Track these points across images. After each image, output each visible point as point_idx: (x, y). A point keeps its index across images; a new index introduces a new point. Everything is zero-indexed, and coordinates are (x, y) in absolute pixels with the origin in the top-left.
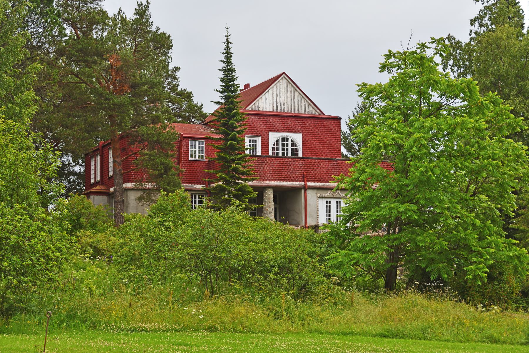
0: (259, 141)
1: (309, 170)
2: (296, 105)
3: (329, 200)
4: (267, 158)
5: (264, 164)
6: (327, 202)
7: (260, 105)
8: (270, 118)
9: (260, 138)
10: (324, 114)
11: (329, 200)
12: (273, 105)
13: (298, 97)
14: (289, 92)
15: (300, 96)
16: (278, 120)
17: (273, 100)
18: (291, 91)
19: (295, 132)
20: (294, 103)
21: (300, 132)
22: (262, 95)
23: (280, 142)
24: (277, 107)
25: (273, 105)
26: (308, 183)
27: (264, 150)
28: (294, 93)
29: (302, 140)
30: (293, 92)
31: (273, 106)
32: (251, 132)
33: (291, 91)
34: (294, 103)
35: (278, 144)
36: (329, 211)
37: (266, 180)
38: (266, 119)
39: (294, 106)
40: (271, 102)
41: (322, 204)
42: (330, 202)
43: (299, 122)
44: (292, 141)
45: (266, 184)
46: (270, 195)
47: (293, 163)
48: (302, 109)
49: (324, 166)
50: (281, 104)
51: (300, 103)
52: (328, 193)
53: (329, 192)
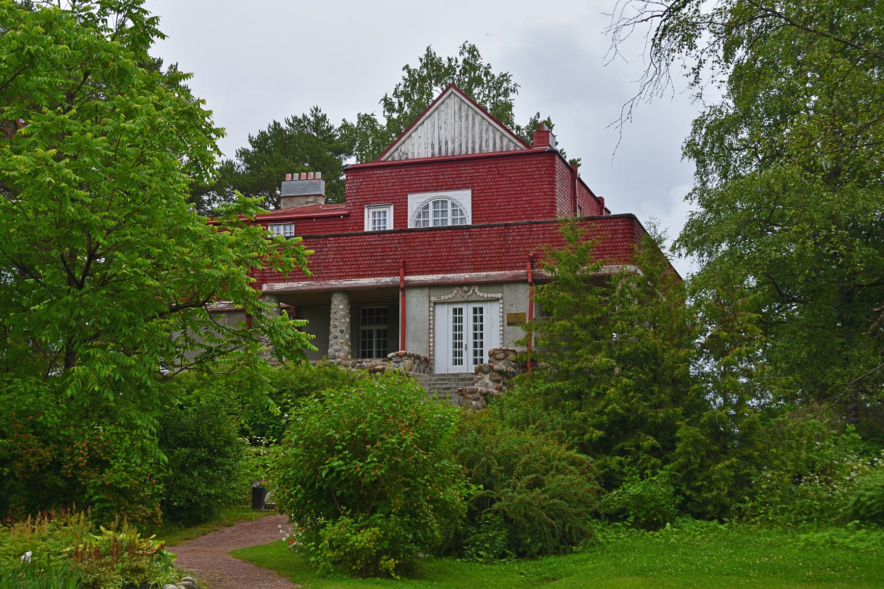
0: (390, 211)
1: (413, 252)
2: (477, 140)
3: (458, 306)
4: (332, 239)
5: (326, 249)
6: (455, 311)
8: (410, 169)
9: (392, 207)
11: (458, 306)
12: (432, 145)
13: (481, 124)
14: (463, 119)
15: (485, 122)
16: (425, 170)
18: (467, 116)
19: (458, 189)
20: (473, 136)
21: (468, 188)
22: (411, 131)
23: (431, 209)
24: (440, 149)
25: (432, 145)
26: (407, 278)
27: (403, 224)
28: (473, 118)
29: (472, 201)
30: (470, 118)
31: (433, 148)
32: (376, 199)
33: (467, 116)
34: (473, 136)
36: (458, 328)
37: (330, 278)
39: (474, 143)
40: (430, 141)
41: (444, 316)
42: (461, 310)
43: (466, 171)
44: (453, 205)
45: (330, 286)
46: (339, 309)
47: (381, 243)
48: (487, 146)
49: (442, 242)
50: (446, 143)
51: (484, 134)
53: (455, 292)
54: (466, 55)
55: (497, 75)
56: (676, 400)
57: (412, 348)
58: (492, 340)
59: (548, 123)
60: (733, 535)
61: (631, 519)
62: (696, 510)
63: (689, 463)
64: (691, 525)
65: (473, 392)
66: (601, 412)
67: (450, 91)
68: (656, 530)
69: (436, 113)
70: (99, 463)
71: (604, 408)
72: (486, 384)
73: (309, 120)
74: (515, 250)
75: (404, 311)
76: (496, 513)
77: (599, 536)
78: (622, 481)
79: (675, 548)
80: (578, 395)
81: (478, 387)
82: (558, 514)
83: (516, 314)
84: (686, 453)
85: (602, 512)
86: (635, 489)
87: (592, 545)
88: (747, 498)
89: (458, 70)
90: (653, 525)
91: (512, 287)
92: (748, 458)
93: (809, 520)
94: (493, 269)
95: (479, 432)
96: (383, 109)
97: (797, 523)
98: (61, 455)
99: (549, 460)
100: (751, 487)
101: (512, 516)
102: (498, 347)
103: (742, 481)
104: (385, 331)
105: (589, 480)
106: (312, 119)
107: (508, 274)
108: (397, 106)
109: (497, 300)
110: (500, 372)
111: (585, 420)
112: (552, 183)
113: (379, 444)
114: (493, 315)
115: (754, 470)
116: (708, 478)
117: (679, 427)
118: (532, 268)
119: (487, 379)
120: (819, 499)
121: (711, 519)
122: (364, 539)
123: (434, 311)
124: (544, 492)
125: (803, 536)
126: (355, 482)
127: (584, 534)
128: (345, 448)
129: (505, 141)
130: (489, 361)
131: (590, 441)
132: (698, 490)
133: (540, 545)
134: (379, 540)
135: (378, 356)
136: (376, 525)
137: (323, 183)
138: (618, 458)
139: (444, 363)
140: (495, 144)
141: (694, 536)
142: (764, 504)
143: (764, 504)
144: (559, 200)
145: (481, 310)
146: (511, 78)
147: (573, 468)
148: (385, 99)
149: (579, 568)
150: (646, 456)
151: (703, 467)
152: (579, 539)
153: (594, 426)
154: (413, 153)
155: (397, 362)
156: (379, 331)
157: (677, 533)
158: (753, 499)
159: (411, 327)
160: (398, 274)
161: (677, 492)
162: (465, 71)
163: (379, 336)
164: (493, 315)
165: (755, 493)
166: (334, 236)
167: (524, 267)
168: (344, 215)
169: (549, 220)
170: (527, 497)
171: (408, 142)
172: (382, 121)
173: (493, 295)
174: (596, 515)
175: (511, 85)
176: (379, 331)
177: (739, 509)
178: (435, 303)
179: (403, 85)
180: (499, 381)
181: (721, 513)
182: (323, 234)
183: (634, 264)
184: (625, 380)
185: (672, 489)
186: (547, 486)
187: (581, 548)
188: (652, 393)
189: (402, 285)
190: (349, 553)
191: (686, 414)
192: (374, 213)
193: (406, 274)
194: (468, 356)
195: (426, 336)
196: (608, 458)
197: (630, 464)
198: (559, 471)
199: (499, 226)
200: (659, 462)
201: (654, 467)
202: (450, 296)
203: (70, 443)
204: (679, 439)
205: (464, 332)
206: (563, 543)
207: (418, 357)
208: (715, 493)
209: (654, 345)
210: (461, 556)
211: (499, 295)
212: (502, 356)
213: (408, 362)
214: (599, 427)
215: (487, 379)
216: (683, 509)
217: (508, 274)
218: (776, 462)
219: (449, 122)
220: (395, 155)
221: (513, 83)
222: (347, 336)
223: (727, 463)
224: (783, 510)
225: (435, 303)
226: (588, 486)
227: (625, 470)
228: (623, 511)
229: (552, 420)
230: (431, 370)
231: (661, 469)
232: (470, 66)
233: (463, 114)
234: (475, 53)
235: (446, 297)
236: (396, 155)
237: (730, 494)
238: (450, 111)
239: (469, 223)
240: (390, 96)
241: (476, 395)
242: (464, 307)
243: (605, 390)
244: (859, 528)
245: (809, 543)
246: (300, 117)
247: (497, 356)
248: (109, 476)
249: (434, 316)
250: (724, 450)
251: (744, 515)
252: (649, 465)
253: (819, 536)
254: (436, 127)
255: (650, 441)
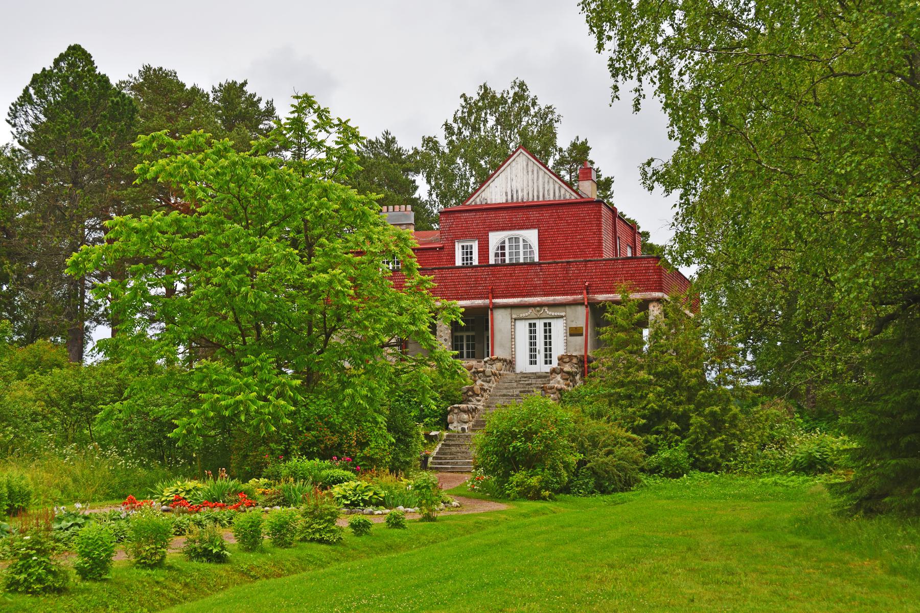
0: (475, 245)
6: (530, 325)
7: (489, 195)
9: (477, 242)
10: (582, 197)
11: (532, 321)
12: (506, 193)
13: (543, 178)
14: (530, 173)
15: (546, 176)
16: (503, 214)
17: (507, 187)
18: (533, 171)
19: (527, 229)
20: (538, 187)
21: (535, 228)
24: (512, 196)
25: (506, 193)
28: (538, 173)
31: (507, 195)
33: (533, 171)
34: (538, 187)
35: (503, 248)
36: (532, 337)
38: (485, 215)
39: (538, 192)
40: (504, 190)
41: (522, 328)
42: (535, 324)
43: (534, 215)
48: (549, 195)
50: (517, 191)
51: (546, 185)
52: (530, 312)
53: (530, 311)
54: (517, 89)
55: (543, 107)
56: (690, 400)
57: (499, 353)
58: (558, 349)
59: (584, 143)
60: (722, 480)
61: (663, 472)
62: (701, 466)
63: (697, 438)
64: (697, 474)
65: (552, 388)
66: (644, 408)
67: (519, 152)
68: (678, 478)
69: (509, 167)
70: (362, 445)
71: (646, 405)
72: (558, 382)
73: (382, 143)
74: (575, 280)
75: (492, 325)
76: (588, 469)
77: (645, 481)
78: (657, 450)
79: (688, 488)
80: (629, 397)
81: (552, 383)
82: (622, 469)
83: (576, 328)
84: (695, 432)
85: (646, 468)
86: (665, 455)
87: (642, 486)
88: (732, 459)
89: (510, 101)
90: (676, 475)
91: (573, 307)
92: (734, 436)
93: (767, 471)
94: (558, 294)
95: (575, 423)
96: (444, 133)
97: (760, 473)
98: (341, 440)
99: (616, 438)
100: (734, 452)
101: (597, 470)
102: (563, 353)
103: (729, 449)
104: (473, 337)
105: (639, 450)
106: (384, 141)
107: (570, 298)
108: (456, 130)
109: (562, 317)
110: (568, 373)
111: (634, 413)
112: (599, 225)
113: (539, 434)
114: (559, 328)
115: (736, 442)
116: (708, 447)
117: (691, 417)
118: (588, 293)
119: (559, 377)
120: (774, 459)
121: (711, 472)
122: (534, 481)
123: (514, 325)
124: (615, 457)
125: (761, 480)
126: (526, 452)
127: (638, 481)
128: (522, 437)
129: (563, 191)
130: (559, 364)
131: (638, 425)
132: (703, 454)
133: (613, 486)
134: (541, 482)
135: (468, 357)
136: (538, 475)
137: (413, 214)
138: (655, 436)
139: (522, 364)
140: (554, 193)
141: (700, 481)
142: (741, 462)
143: (741, 462)
144: (604, 237)
145: (550, 324)
146: (555, 110)
147: (629, 443)
148: (446, 124)
149: (636, 498)
150: (671, 434)
151: (706, 441)
152: (634, 483)
153: (640, 416)
154: (492, 200)
155: (491, 365)
156: (468, 337)
157: (690, 480)
158: (735, 459)
159: (498, 337)
160: (487, 298)
161: (691, 456)
162: (515, 101)
163: (468, 340)
164: (559, 328)
165: (737, 456)
166: (438, 269)
167: (581, 293)
168: (440, 248)
169: (599, 259)
170: (606, 460)
171: (488, 190)
172: (443, 143)
173: (559, 314)
174: (642, 470)
175: (555, 117)
176: (468, 337)
177: (727, 465)
178: (515, 319)
179: (460, 111)
180: (567, 379)
181: (717, 468)
182: (430, 267)
183: (662, 292)
184: (659, 388)
185: (687, 454)
186: (616, 453)
187: (635, 488)
188: (675, 395)
189: (491, 306)
190: (526, 489)
191: (696, 409)
192: (463, 247)
193: (494, 298)
194: (541, 358)
195: (510, 343)
196: (649, 436)
197: (662, 439)
198: (622, 445)
199: (562, 262)
200: (679, 438)
201: (676, 441)
202: (527, 314)
203: (345, 432)
204: (692, 424)
205: (537, 341)
206: (625, 486)
207: (505, 360)
208: (713, 456)
209: (676, 366)
210: (569, 493)
211: (563, 314)
212: (567, 360)
213: (499, 365)
214: (643, 417)
215: (559, 377)
216: (694, 466)
217: (570, 298)
218: (750, 437)
219: (519, 175)
220: (477, 200)
221: (556, 114)
222: (450, 344)
223: (720, 438)
224: (753, 466)
225: (515, 319)
226: (639, 453)
227: (659, 443)
228: (658, 467)
229: (614, 413)
230: (514, 368)
231: (681, 442)
232: (519, 97)
233: (530, 169)
234: (524, 87)
235: (524, 315)
236: (478, 200)
237: (722, 456)
238: (520, 167)
239: (537, 259)
240: (450, 121)
241: (554, 390)
242: (537, 322)
243: (647, 394)
244: (793, 474)
245: (763, 483)
246: (374, 140)
247: (565, 360)
248: (366, 451)
249: (515, 329)
250: (719, 430)
251: (730, 469)
252: (674, 440)
253: (769, 480)
254: (509, 178)
255: (674, 426)
